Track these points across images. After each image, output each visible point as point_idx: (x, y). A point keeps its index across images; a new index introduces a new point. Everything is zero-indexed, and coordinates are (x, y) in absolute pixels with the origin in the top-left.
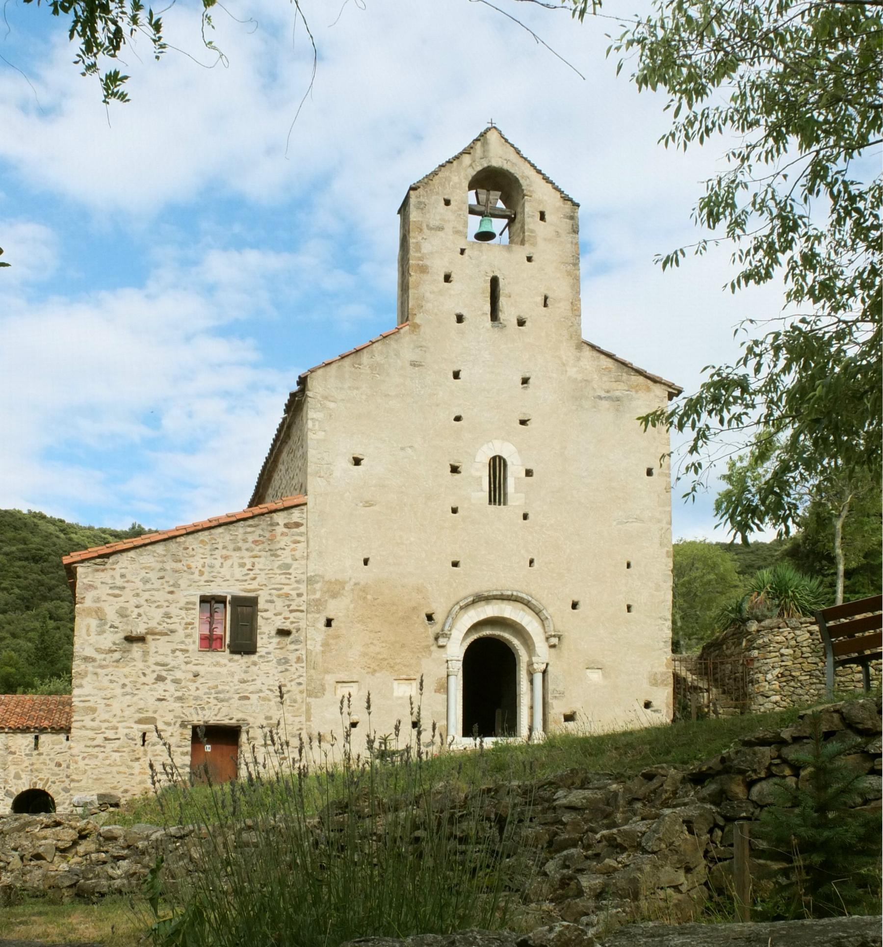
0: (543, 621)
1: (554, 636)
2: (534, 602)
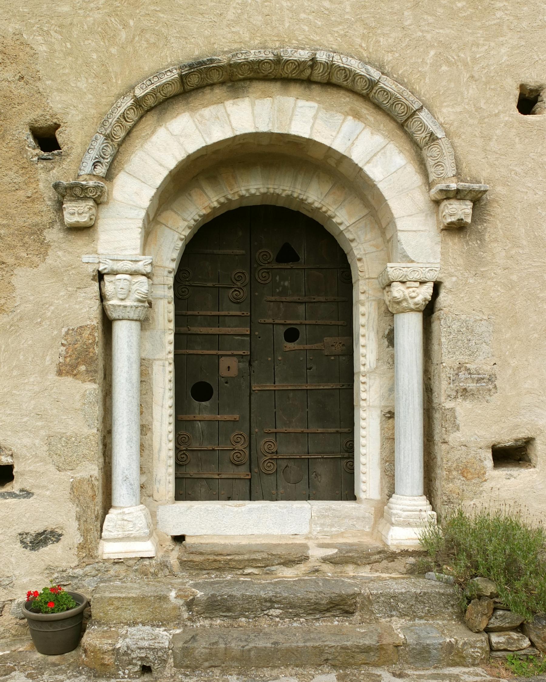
0: (419, 149)
1: (458, 195)
2: (388, 84)
